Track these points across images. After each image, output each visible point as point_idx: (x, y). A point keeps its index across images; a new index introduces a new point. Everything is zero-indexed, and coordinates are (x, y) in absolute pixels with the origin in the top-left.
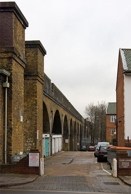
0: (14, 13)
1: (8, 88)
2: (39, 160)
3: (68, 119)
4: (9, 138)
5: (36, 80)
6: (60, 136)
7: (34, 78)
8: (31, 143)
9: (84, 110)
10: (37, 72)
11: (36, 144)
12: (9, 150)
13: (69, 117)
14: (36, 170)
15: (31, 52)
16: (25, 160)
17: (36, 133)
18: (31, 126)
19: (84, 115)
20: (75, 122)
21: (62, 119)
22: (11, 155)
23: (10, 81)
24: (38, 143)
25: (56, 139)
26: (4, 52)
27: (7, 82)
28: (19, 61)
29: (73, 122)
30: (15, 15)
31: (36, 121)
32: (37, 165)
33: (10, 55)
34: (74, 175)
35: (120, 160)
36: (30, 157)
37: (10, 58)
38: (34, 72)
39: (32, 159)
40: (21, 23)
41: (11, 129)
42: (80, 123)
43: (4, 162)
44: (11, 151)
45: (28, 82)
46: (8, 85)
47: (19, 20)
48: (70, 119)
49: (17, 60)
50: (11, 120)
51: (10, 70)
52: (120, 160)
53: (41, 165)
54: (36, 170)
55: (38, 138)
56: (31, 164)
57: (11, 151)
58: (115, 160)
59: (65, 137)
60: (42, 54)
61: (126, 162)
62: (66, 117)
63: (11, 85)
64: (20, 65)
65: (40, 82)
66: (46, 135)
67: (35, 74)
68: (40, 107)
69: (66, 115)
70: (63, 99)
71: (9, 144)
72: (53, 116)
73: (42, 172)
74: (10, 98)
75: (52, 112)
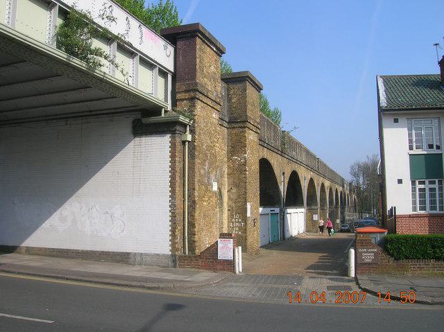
0: (199, 37)
1: (189, 142)
2: (232, 250)
3: (316, 184)
4: (191, 215)
5: (245, 127)
6: (303, 210)
7: (241, 125)
8: (238, 222)
9: (349, 170)
10: (246, 116)
11: (246, 224)
12: (192, 234)
13: (318, 181)
14: (230, 264)
15: (236, 88)
16: (214, 249)
17: (246, 208)
18: (239, 197)
19: (348, 178)
20: (331, 189)
21: (304, 185)
22: (194, 242)
23: (192, 132)
24: (249, 222)
25: (293, 214)
26: (185, 90)
27: (188, 133)
28: (209, 102)
29: (326, 188)
30: (201, 39)
31: (245, 188)
32: (230, 257)
33: (192, 94)
34: (25, 262)
35: (360, 250)
36: (220, 245)
37: (192, 99)
38: (241, 117)
39: (223, 248)
40: (213, 49)
41: (194, 202)
42: (340, 189)
43: (184, 253)
44: (195, 235)
45: (234, 132)
46: (189, 138)
47: (209, 46)
48: (320, 184)
49: (205, 100)
50: (194, 189)
51: (192, 117)
52: (360, 250)
53: (237, 257)
54: (230, 264)
55: (249, 214)
56: (221, 256)
57: (195, 235)
58: (352, 251)
59: (311, 211)
60: (255, 90)
61: (370, 252)
62: (311, 181)
63: (193, 137)
64: (212, 107)
65: (252, 130)
66: (273, 209)
67: (242, 119)
68: (253, 169)
69: (311, 178)
70: (304, 154)
71: (192, 225)
72: (287, 181)
73: (239, 268)
74: (192, 156)
75: (284, 173)
